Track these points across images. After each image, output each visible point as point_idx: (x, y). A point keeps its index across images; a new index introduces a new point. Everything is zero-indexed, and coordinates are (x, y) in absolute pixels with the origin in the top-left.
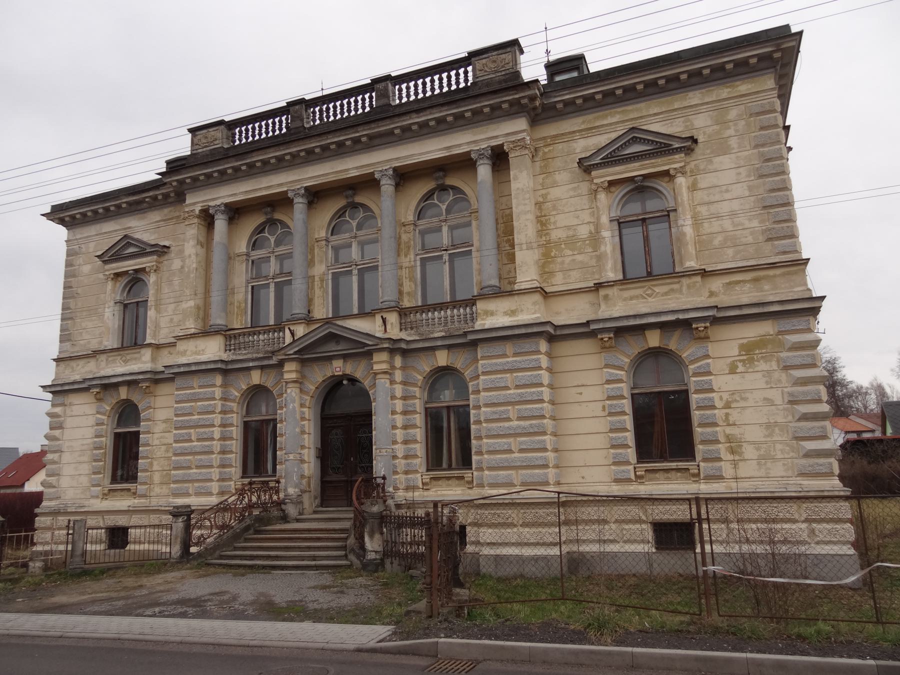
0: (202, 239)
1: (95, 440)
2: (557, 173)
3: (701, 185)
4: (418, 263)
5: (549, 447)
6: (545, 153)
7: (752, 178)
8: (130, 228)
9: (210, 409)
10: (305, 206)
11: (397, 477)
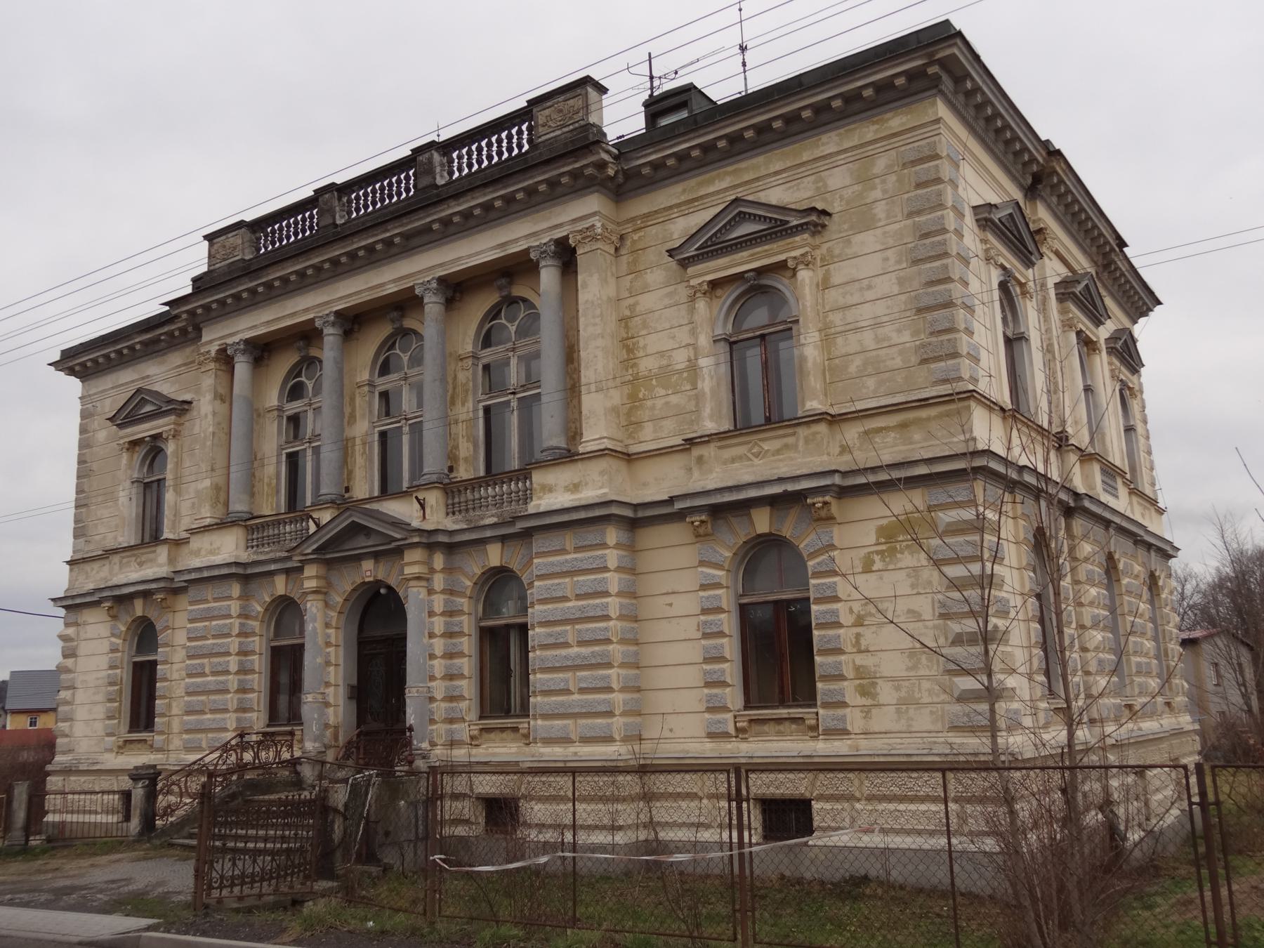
0: (221, 391)
1: (110, 672)
2: (648, 271)
3: (836, 279)
4: (481, 413)
5: (615, 686)
6: (634, 242)
7: (904, 265)
8: (148, 376)
9: (226, 631)
10: (443, 308)
11: (434, 727)
